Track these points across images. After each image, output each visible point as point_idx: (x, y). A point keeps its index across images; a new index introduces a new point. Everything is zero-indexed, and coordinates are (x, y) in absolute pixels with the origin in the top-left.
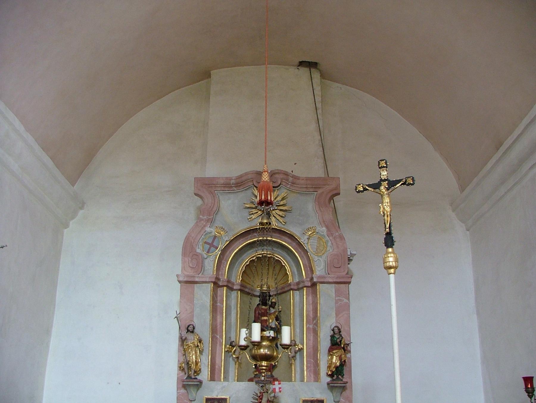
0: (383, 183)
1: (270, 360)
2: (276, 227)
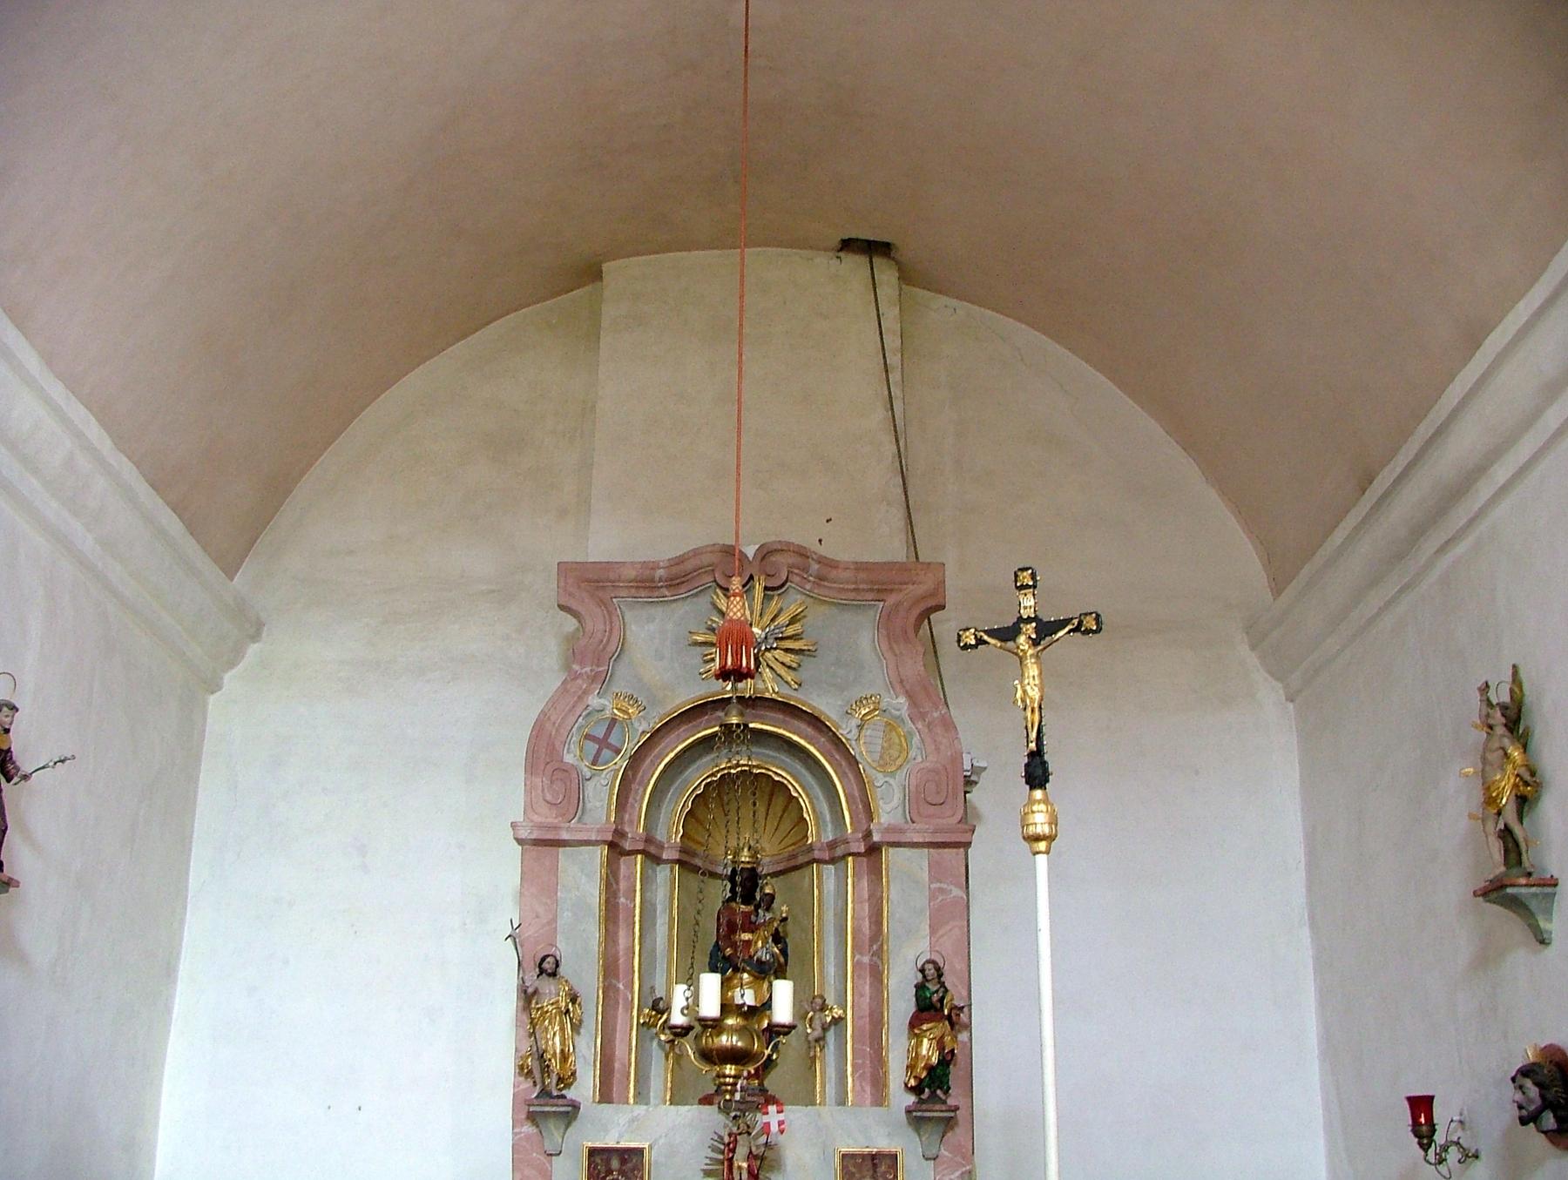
0: (1024, 627)
1: (744, 1062)
2: (774, 696)
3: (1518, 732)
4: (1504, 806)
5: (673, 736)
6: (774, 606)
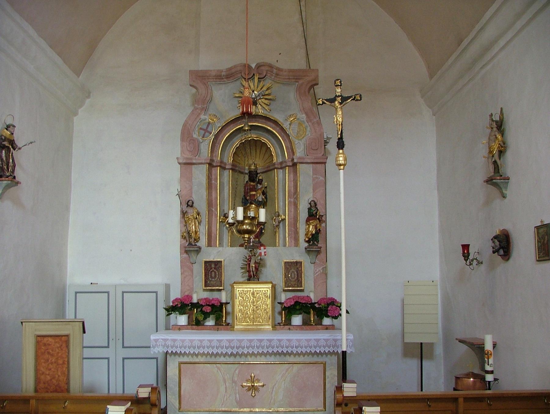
3: (501, 129)
4: (495, 154)
5: (229, 127)
6: (261, 84)
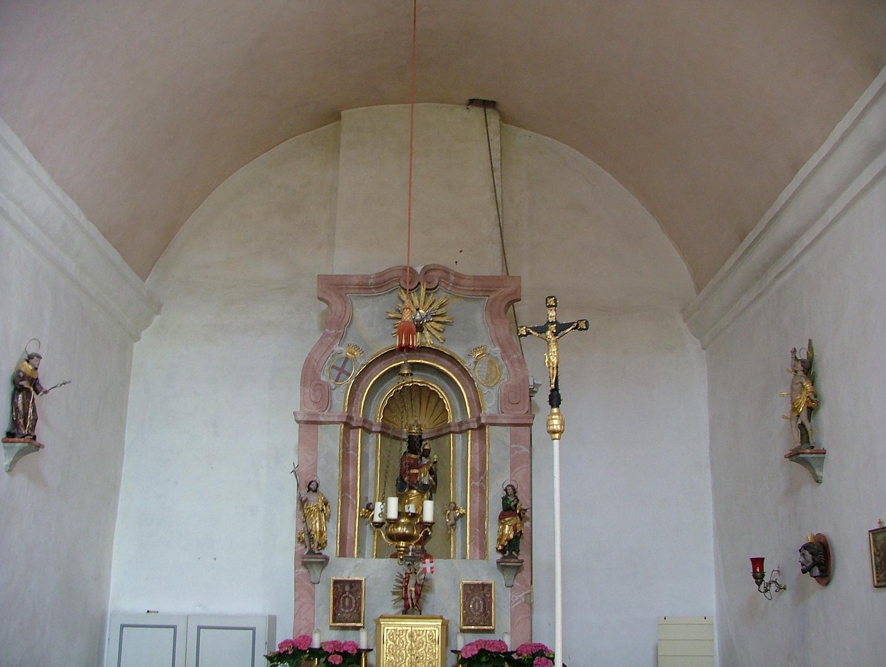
2: (431, 346)
6: (431, 298)
